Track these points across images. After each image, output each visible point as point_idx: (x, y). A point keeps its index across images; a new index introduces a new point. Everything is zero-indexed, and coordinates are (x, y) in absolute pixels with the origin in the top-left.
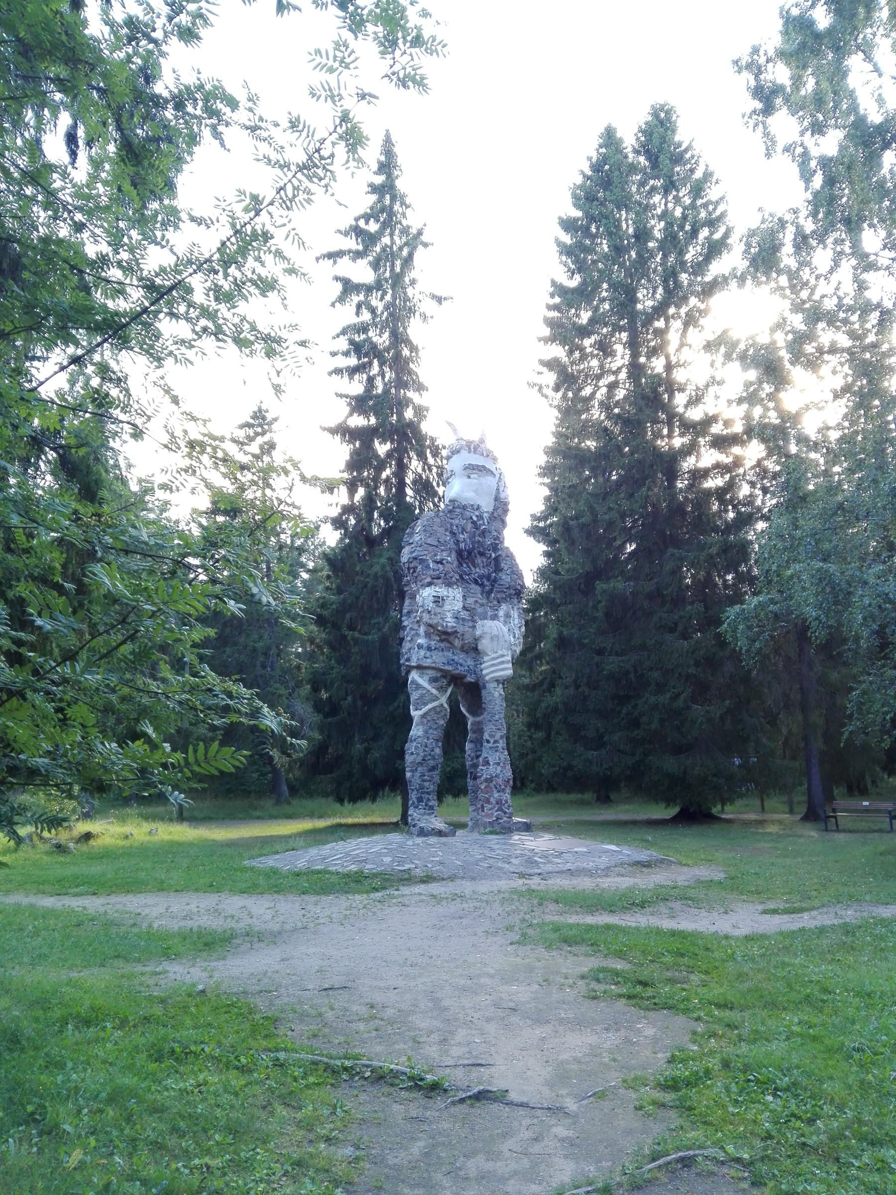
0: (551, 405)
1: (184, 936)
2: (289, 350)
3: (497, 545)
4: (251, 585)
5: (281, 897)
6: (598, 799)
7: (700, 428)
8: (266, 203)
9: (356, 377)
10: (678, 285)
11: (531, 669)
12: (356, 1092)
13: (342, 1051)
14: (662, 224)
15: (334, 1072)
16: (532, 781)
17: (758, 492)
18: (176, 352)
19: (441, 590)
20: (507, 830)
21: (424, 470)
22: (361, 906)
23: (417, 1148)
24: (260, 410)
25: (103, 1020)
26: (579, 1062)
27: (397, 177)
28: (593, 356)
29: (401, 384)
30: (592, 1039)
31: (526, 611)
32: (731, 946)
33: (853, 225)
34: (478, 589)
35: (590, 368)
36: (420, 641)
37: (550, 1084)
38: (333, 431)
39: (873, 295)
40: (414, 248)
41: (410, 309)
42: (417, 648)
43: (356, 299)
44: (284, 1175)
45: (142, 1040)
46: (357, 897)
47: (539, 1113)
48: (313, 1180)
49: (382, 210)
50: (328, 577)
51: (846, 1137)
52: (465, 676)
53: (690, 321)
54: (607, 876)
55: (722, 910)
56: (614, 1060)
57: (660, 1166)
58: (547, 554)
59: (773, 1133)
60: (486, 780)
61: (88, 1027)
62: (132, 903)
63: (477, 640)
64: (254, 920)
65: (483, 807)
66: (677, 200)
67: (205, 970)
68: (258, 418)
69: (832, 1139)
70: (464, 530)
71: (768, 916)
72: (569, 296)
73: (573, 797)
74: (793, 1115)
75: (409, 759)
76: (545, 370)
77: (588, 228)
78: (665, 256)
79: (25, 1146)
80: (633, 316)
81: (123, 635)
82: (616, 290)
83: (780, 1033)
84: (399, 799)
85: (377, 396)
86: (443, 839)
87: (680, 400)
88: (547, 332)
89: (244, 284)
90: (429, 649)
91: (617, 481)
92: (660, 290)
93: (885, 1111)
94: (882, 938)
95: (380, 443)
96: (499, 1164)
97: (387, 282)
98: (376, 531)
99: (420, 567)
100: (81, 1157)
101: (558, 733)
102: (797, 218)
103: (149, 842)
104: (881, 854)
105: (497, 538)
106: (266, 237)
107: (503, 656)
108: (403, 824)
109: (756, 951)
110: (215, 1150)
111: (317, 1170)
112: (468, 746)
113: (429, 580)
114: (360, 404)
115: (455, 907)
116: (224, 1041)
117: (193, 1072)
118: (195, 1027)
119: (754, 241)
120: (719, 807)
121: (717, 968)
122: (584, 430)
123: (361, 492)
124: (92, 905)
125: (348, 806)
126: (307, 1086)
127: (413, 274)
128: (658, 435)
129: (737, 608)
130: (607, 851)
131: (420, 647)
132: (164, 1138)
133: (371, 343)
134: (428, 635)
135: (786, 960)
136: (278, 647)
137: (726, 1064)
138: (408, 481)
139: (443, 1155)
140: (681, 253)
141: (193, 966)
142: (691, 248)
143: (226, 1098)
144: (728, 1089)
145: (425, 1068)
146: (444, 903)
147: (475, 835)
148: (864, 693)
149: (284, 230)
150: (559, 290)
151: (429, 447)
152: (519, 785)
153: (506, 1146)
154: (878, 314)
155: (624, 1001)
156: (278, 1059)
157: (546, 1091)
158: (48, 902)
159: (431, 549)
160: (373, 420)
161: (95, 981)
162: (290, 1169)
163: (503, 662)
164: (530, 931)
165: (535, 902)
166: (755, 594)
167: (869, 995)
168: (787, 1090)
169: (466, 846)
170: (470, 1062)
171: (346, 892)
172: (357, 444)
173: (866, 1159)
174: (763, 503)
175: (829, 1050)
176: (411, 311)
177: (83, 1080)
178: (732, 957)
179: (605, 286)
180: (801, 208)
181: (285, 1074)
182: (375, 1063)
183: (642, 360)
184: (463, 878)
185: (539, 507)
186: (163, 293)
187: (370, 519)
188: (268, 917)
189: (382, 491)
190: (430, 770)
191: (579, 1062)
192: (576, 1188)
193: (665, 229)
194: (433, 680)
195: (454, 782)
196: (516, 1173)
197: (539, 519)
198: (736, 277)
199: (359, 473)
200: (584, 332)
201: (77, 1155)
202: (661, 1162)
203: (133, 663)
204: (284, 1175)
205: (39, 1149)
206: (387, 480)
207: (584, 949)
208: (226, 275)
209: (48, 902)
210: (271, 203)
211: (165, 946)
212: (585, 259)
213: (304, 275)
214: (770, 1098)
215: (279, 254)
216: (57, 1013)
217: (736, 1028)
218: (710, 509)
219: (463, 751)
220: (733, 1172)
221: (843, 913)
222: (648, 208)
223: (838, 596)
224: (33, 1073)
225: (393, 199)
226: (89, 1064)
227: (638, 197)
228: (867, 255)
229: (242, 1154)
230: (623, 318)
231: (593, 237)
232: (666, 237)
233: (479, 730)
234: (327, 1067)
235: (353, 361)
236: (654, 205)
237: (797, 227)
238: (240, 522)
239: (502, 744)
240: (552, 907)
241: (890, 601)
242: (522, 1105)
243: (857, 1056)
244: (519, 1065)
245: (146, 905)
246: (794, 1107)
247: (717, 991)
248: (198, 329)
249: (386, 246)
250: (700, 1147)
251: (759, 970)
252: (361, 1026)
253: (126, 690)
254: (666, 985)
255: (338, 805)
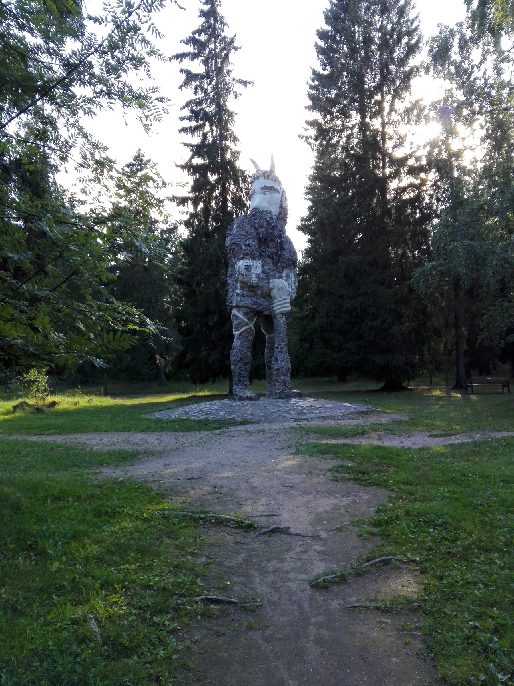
0: (313, 149)
1: (110, 454)
2: (153, 104)
3: (282, 231)
4: (135, 240)
5: (164, 433)
6: (339, 380)
7: (401, 163)
8: (135, 7)
9: (196, 133)
10: (389, 72)
11: (301, 308)
12: (207, 530)
13: (199, 510)
14: (380, 34)
15: (195, 520)
16: (302, 371)
17: (434, 201)
18: (85, 107)
19: (249, 262)
20: (289, 396)
21: (238, 191)
22: (208, 437)
23: (240, 558)
24: (139, 155)
25: (67, 497)
26: (328, 513)
27: (218, 6)
28: (338, 118)
29: (222, 137)
30: (334, 501)
31: (299, 275)
32: (411, 454)
33: (496, 32)
34: (270, 261)
35: (336, 126)
36: (238, 291)
37: (311, 524)
38: (183, 167)
39: (505, 77)
40: (229, 51)
41: (227, 90)
42: (236, 295)
43: (194, 84)
44: (169, 572)
45: (89, 507)
46: (206, 433)
47: (306, 539)
48: (185, 574)
49: (209, 27)
50: (184, 256)
51: (472, 548)
52: (264, 311)
53: (397, 95)
54: (343, 419)
55: (407, 435)
56: (347, 512)
57: (371, 564)
58: (310, 241)
59: (433, 547)
60: (276, 369)
61: (59, 501)
62: (81, 438)
63: (270, 290)
64: (149, 445)
65: (275, 384)
66: (389, 20)
67: (123, 471)
68: (138, 160)
69: (464, 549)
70: (262, 226)
71: (432, 438)
72: (324, 80)
73: (325, 379)
74: (444, 538)
75: (232, 358)
76: (309, 127)
77: (335, 37)
78: (381, 54)
79: (28, 562)
80: (362, 91)
81: (63, 277)
82: (352, 77)
83: (437, 497)
84: (228, 382)
85: (209, 145)
86: (253, 402)
87: (389, 145)
88: (310, 103)
89: (124, 61)
90: (243, 296)
91: (352, 196)
92: (379, 76)
93: (493, 535)
94: (495, 448)
95: (212, 174)
96: (285, 564)
97: (213, 73)
98: (210, 229)
99: (237, 248)
100: (58, 565)
101: (317, 344)
102: (461, 29)
103: (88, 406)
104: (496, 405)
105: (281, 231)
106: (136, 29)
107: (285, 299)
108: (231, 395)
109: (425, 455)
110: (131, 561)
111: (187, 570)
112: (266, 351)
113: (242, 256)
114: (198, 150)
115: (259, 437)
116: (134, 506)
117: (118, 522)
118: (118, 500)
119: (435, 45)
120: (407, 382)
121: (403, 465)
122: (332, 165)
123: (201, 205)
124: (59, 439)
125: (199, 386)
126: (181, 528)
127: (229, 67)
128: (377, 167)
129: (420, 269)
130: (344, 406)
131: (238, 295)
132: (103, 556)
133: (204, 111)
134: (242, 288)
135: (442, 460)
136: (156, 298)
137: (407, 513)
138: (229, 198)
139: (255, 560)
140: (392, 52)
141: (116, 469)
142: (397, 50)
143: (137, 535)
144: (408, 526)
145: (244, 517)
146: (254, 435)
147: (271, 400)
148: (491, 316)
149: (147, 25)
150: (317, 76)
151: (241, 176)
152: (295, 373)
153: (288, 556)
154: (508, 89)
155: (352, 482)
156: (164, 514)
157: (310, 528)
158: (34, 438)
159: (243, 238)
160: (207, 161)
161: (63, 478)
162: (172, 569)
163: (285, 303)
164: (301, 448)
165: (304, 433)
166: (430, 261)
167: (487, 477)
168: (440, 526)
169: (266, 406)
170: (268, 514)
171: (200, 430)
172: (198, 175)
173: (482, 558)
174: (437, 208)
175: (465, 505)
176: (228, 91)
177: (57, 528)
178: (412, 459)
179: (345, 74)
180: (464, 22)
181: (168, 522)
182: (217, 515)
183: (367, 120)
184: (264, 422)
185: (306, 213)
186: (75, 69)
187: (207, 221)
188: (157, 444)
189: (213, 204)
190: (244, 365)
191: (328, 513)
192: (326, 575)
193: (382, 37)
194: (245, 314)
195: (258, 372)
196: (294, 569)
197: (306, 220)
198: (424, 67)
199: (199, 193)
200: (333, 103)
201: (56, 565)
202: (372, 562)
203: (70, 294)
204: (169, 572)
205: (36, 562)
206: (216, 197)
207: (330, 456)
208: (113, 57)
209: (34, 438)
210: (139, 8)
211: (101, 459)
212: (333, 56)
213: (160, 55)
214: (432, 530)
215: (144, 41)
216: (42, 494)
217: (414, 495)
218: (406, 211)
219: (263, 354)
220: (411, 567)
221: (474, 436)
222: (372, 24)
223: (478, 260)
224: (29, 524)
225: (216, 20)
226: (60, 519)
227: (365, 17)
228: (503, 52)
229: (146, 563)
230: (356, 94)
231: (338, 42)
232: (382, 43)
233: (273, 342)
234: (191, 518)
235: (194, 124)
236: (375, 22)
237: (461, 35)
238: (132, 220)
239: (285, 349)
240: (313, 435)
241: (509, 263)
242: (297, 535)
243: (480, 508)
244: (295, 515)
245: (89, 439)
246: (444, 534)
247: (403, 476)
248: (97, 90)
249: (212, 50)
250: (394, 555)
251: (426, 465)
252: (210, 497)
253: (68, 311)
254: (375, 474)
255: (194, 385)
